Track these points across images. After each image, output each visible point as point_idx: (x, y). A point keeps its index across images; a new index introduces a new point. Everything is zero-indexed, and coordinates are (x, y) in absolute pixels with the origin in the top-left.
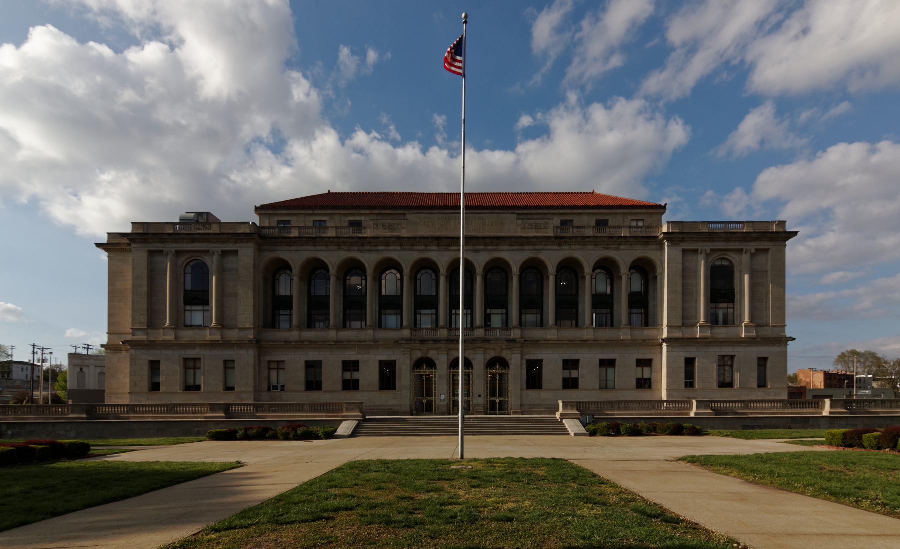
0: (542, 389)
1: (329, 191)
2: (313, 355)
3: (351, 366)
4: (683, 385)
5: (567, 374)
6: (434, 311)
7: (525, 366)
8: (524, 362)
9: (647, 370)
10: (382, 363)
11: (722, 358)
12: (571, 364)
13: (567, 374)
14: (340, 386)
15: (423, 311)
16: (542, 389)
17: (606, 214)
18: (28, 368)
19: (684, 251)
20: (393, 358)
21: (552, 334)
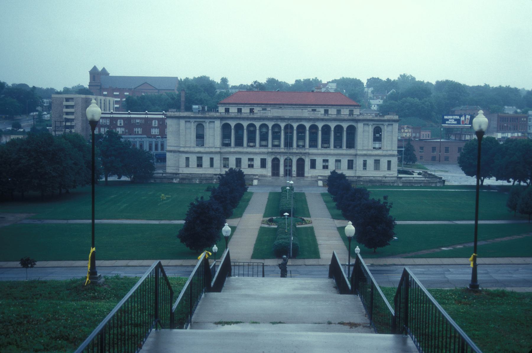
0: (379, 170)
1: (316, 78)
2: (239, 156)
3: (251, 160)
4: (362, 169)
5: (250, 163)
6: (230, 140)
7: (310, 161)
8: (310, 160)
9: (227, 162)
10: (349, 161)
11: (375, 160)
12: (325, 161)
13: (324, 164)
14: (247, 167)
15: (275, 140)
16: (379, 170)
17: (341, 108)
18: (368, 162)
19: (364, 124)
20: (265, 158)
21: (320, 151)
